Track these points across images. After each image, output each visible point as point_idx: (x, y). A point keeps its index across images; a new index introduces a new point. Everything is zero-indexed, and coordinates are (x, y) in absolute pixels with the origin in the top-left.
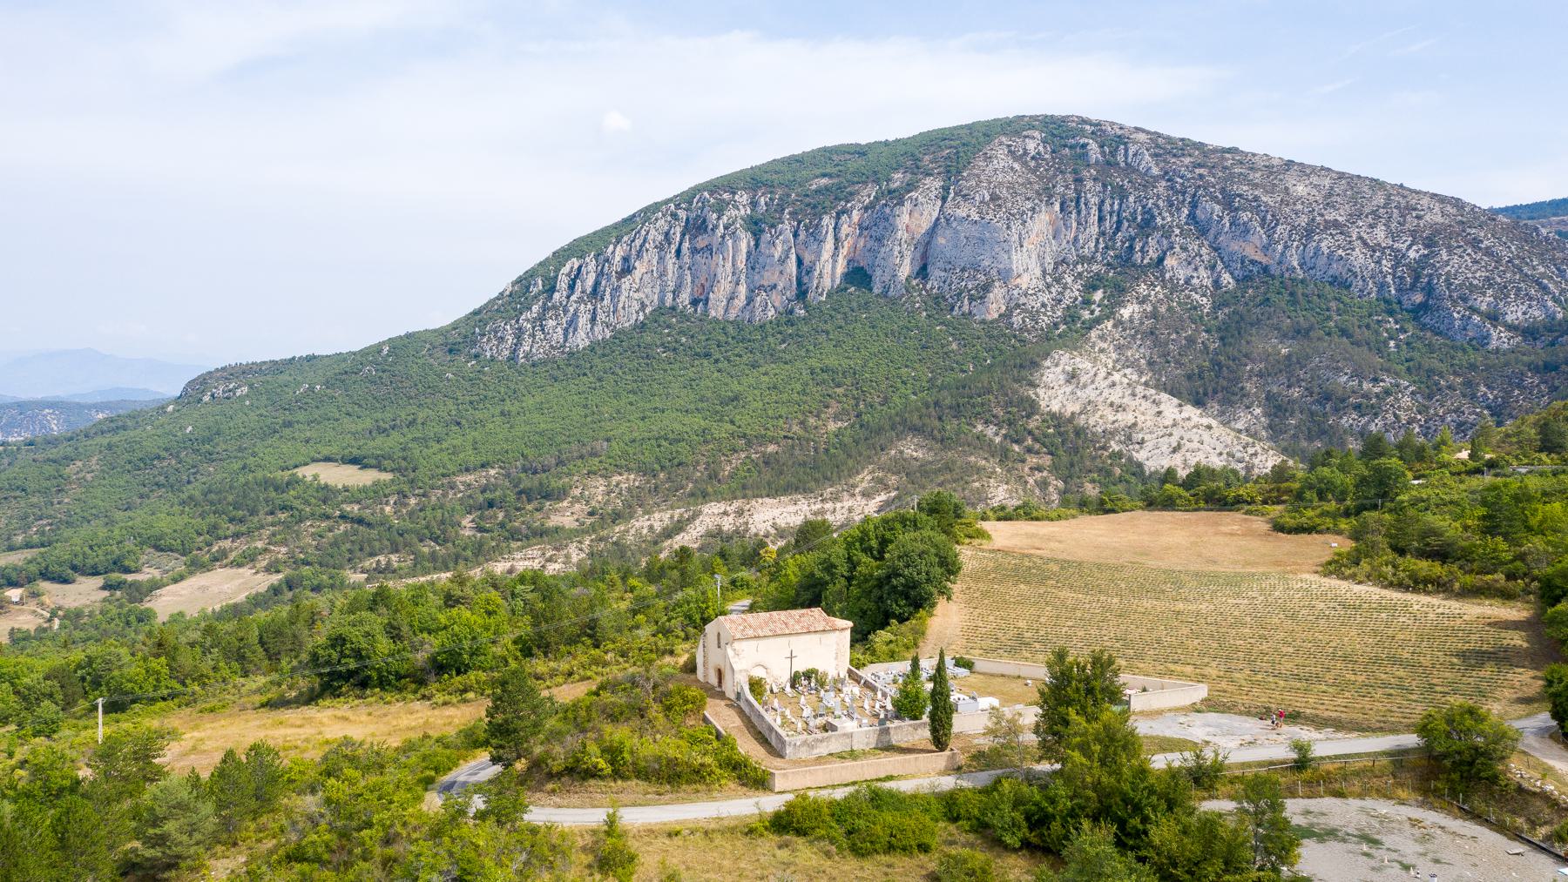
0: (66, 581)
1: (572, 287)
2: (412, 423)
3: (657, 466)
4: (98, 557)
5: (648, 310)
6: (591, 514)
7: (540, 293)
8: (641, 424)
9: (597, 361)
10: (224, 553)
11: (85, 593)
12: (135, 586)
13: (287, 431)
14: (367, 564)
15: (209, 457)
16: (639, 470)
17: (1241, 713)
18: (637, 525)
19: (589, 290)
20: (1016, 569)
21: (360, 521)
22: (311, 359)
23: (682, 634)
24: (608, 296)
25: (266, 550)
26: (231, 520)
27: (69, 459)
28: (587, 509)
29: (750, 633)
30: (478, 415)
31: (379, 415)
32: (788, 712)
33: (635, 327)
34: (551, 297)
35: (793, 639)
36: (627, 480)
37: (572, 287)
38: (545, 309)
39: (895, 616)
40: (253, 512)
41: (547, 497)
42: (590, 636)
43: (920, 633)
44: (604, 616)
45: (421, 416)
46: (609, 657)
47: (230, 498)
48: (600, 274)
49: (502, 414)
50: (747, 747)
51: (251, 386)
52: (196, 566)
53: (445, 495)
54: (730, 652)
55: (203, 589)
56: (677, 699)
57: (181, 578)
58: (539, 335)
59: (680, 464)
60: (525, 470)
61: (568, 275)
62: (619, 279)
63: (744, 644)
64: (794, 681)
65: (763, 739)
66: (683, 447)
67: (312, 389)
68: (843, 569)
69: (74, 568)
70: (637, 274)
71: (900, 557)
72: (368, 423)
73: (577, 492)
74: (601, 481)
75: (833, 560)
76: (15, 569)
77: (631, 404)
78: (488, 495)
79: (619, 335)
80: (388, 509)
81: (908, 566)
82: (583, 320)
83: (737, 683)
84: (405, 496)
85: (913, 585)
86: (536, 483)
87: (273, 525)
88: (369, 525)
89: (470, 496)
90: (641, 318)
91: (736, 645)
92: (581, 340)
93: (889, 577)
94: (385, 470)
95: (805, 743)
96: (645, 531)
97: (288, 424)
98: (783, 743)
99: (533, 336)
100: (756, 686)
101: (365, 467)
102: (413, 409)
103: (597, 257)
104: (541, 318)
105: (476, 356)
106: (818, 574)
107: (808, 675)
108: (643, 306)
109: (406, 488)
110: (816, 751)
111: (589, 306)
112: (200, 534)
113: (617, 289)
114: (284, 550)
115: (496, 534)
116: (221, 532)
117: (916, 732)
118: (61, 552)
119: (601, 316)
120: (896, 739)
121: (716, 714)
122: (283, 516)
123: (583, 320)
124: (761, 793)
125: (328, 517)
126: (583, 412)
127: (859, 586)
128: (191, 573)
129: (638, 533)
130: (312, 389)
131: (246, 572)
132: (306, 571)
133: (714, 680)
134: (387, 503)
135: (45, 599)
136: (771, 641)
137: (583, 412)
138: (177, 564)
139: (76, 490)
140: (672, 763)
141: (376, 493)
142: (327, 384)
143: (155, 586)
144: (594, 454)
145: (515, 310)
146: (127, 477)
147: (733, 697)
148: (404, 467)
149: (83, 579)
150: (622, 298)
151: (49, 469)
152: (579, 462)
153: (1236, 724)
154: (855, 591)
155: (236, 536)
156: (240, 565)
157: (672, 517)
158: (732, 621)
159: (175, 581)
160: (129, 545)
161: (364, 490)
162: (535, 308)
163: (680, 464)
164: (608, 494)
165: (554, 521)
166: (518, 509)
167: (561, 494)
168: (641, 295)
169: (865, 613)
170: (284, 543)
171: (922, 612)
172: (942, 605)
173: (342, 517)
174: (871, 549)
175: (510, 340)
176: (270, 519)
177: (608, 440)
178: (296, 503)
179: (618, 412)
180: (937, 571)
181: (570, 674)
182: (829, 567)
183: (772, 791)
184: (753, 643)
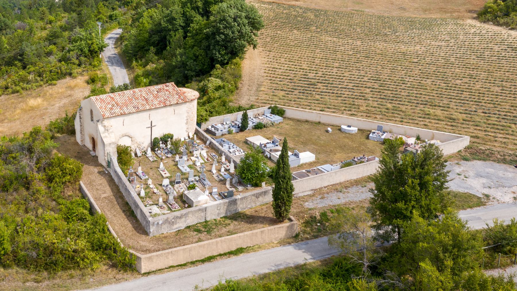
17: (499, 161)
20: (288, 16)
23: (77, 62)
29: (117, 110)
32: (150, 182)
35: (152, 112)
39: (218, 62)
42: (20, 61)
43: (237, 77)
44: (30, 50)
46: (31, 77)
50: (118, 227)
54: (101, 128)
56: (57, 170)
64: (154, 145)
65: (130, 211)
68: (180, 22)
71: (221, 20)
75: (174, 15)
81: (225, 28)
83: (108, 152)
85: (228, 40)
91: (106, 123)
93: (214, 34)
95: (166, 221)
98: (148, 222)
100: (123, 154)
106: (164, 24)
107: (165, 139)
110: (175, 226)
117: (258, 198)
120: (242, 208)
121: (90, 184)
124: (128, 275)
127: (193, 37)
133: (90, 146)
136: (135, 116)
140: (50, 251)
147: (104, 164)
153: (501, 173)
154: (190, 41)
158: (102, 100)
169: (197, 57)
171: (237, 60)
172: (249, 51)
174: (198, 8)
180: (247, 29)
181: (7, 88)
182: (171, 20)
183: (139, 272)
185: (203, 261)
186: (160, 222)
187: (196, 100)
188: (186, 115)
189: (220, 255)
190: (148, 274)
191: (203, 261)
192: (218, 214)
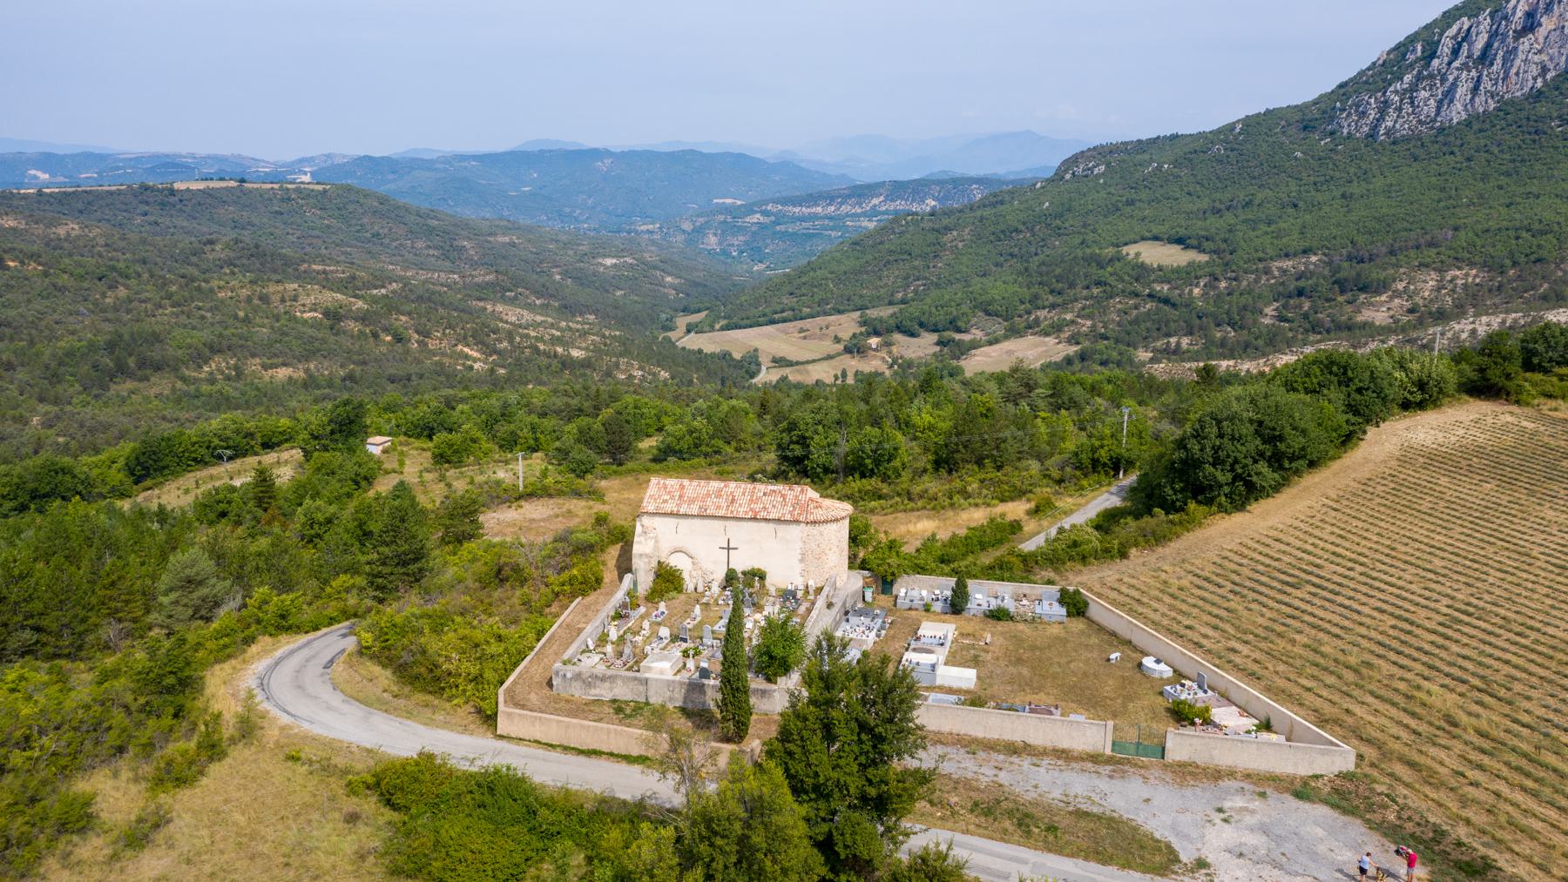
0: (913, 335)
1: (1455, 52)
2: (1248, 204)
3: (1508, 262)
4: (940, 317)
5: (1548, 77)
6: (1411, 311)
7: (1418, 60)
8: (1504, 211)
9: (1471, 137)
10: (1037, 322)
11: (921, 348)
12: (959, 344)
13: (1128, 209)
14: (1159, 344)
15: (1059, 232)
16: (1484, 264)
18: (1457, 327)
19: (1477, 54)
21: (1166, 301)
22: (1175, 137)
24: (1499, 61)
25: (1073, 322)
26: (1052, 292)
27: (948, 229)
28: (1408, 305)
30: (1320, 197)
31: (1218, 195)
33: (1527, 97)
34: (1428, 65)
35: (730, 524)
36: (1463, 276)
37: (1455, 52)
38: (1419, 78)
40: (1072, 286)
41: (1363, 289)
45: (1260, 196)
47: (1058, 271)
48: (1493, 35)
49: (1343, 196)
51: (1108, 165)
52: (1014, 333)
53: (1257, 281)
55: (1010, 352)
57: (996, 341)
58: (1407, 108)
59: (1539, 260)
60: (1350, 258)
61: (1454, 37)
62: (1516, 39)
63: (657, 521)
66: (1548, 242)
67: (1159, 168)
69: (921, 325)
70: (1542, 32)
72: (1205, 204)
73: (1400, 286)
74: (1434, 275)
76: (881, 321)
77: (1500, 187)
78: (1302, 283)
79: (1505, 107)
80: (1196, 291)
82: (1462, 91)
84: (1216, 279)
86: (1354, 273)
87: (1086, 299)
88: (1174, 305)
89: (1283, 284)
90: (1539, 84)
92: (1457, 112)
94: (1204, 251)
96: (1464, 336)
97: (1130, 203)
99: (1400, 109)
101: (1187, 247)
102: (1251, 189)
103: (1492, 15)
104: (1413, 88)
105: (1332, 133)
108: (1544, 70)
109: (1218, 271)
110: (593, 691)
111: (1474, 73)
112: (1022, 303)
113: (1511, 53)
114: (1089, 323)
115: (1295, 324)
116: (1040, 302)
118: (914, 310)
119: (1487, 84)
122: (1096, 291)
123: (1462, 91)
125: (1137, 295)
126: (1435, 194)
128: (1006, 338)
129: (1456, 338)
130: (1159, 168)
131: (1051, 340)
132: (1102, 345)
134: (1197, 285)
135: (894, 349)
136: (698, 522)
137: (1435, 194)
138: (999, 327)
139: (948, 256)
141: (1188, 275)
142: (1176, 163)
143: (975, 345)
144: (1431, 244)
145: (1384, 80)
146: (989, 247)
148: (1223, 250)
149: (926, 334)
150: (1518, 62)
151: (931, 237)
152: (1412, 253)
155: (1053, 306)
156: (1047, 334)
157: (1504, 322)
159: (990, 343)
160: (965, 308)
161: (1177, 270)
162: (1408, 78)
163: (1539, 260)
164: (1439, 289)
165: (1366, 315)
166: (1328, 300)
167: (1382, 287)
168: (1544, 57)
170: (1090, 317)
173: (1150, 296)
175: (1372, 114)
176: (1085, 292)
177: (1456, 229)
178: (1111, 280)
179: (1481, 197)
184: (672, 521)
185: (581, 752)
186: (569, 675)
187: (847, 521)
188: (799, 544)
189: (611, 754)
190: (501, 737)
191: (581, 752)
192: (671, 699)
